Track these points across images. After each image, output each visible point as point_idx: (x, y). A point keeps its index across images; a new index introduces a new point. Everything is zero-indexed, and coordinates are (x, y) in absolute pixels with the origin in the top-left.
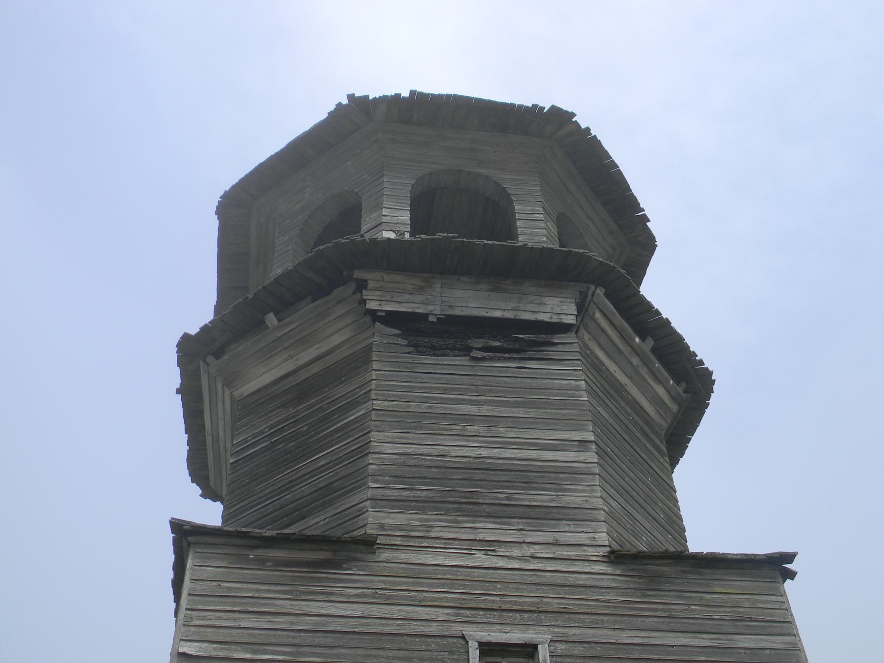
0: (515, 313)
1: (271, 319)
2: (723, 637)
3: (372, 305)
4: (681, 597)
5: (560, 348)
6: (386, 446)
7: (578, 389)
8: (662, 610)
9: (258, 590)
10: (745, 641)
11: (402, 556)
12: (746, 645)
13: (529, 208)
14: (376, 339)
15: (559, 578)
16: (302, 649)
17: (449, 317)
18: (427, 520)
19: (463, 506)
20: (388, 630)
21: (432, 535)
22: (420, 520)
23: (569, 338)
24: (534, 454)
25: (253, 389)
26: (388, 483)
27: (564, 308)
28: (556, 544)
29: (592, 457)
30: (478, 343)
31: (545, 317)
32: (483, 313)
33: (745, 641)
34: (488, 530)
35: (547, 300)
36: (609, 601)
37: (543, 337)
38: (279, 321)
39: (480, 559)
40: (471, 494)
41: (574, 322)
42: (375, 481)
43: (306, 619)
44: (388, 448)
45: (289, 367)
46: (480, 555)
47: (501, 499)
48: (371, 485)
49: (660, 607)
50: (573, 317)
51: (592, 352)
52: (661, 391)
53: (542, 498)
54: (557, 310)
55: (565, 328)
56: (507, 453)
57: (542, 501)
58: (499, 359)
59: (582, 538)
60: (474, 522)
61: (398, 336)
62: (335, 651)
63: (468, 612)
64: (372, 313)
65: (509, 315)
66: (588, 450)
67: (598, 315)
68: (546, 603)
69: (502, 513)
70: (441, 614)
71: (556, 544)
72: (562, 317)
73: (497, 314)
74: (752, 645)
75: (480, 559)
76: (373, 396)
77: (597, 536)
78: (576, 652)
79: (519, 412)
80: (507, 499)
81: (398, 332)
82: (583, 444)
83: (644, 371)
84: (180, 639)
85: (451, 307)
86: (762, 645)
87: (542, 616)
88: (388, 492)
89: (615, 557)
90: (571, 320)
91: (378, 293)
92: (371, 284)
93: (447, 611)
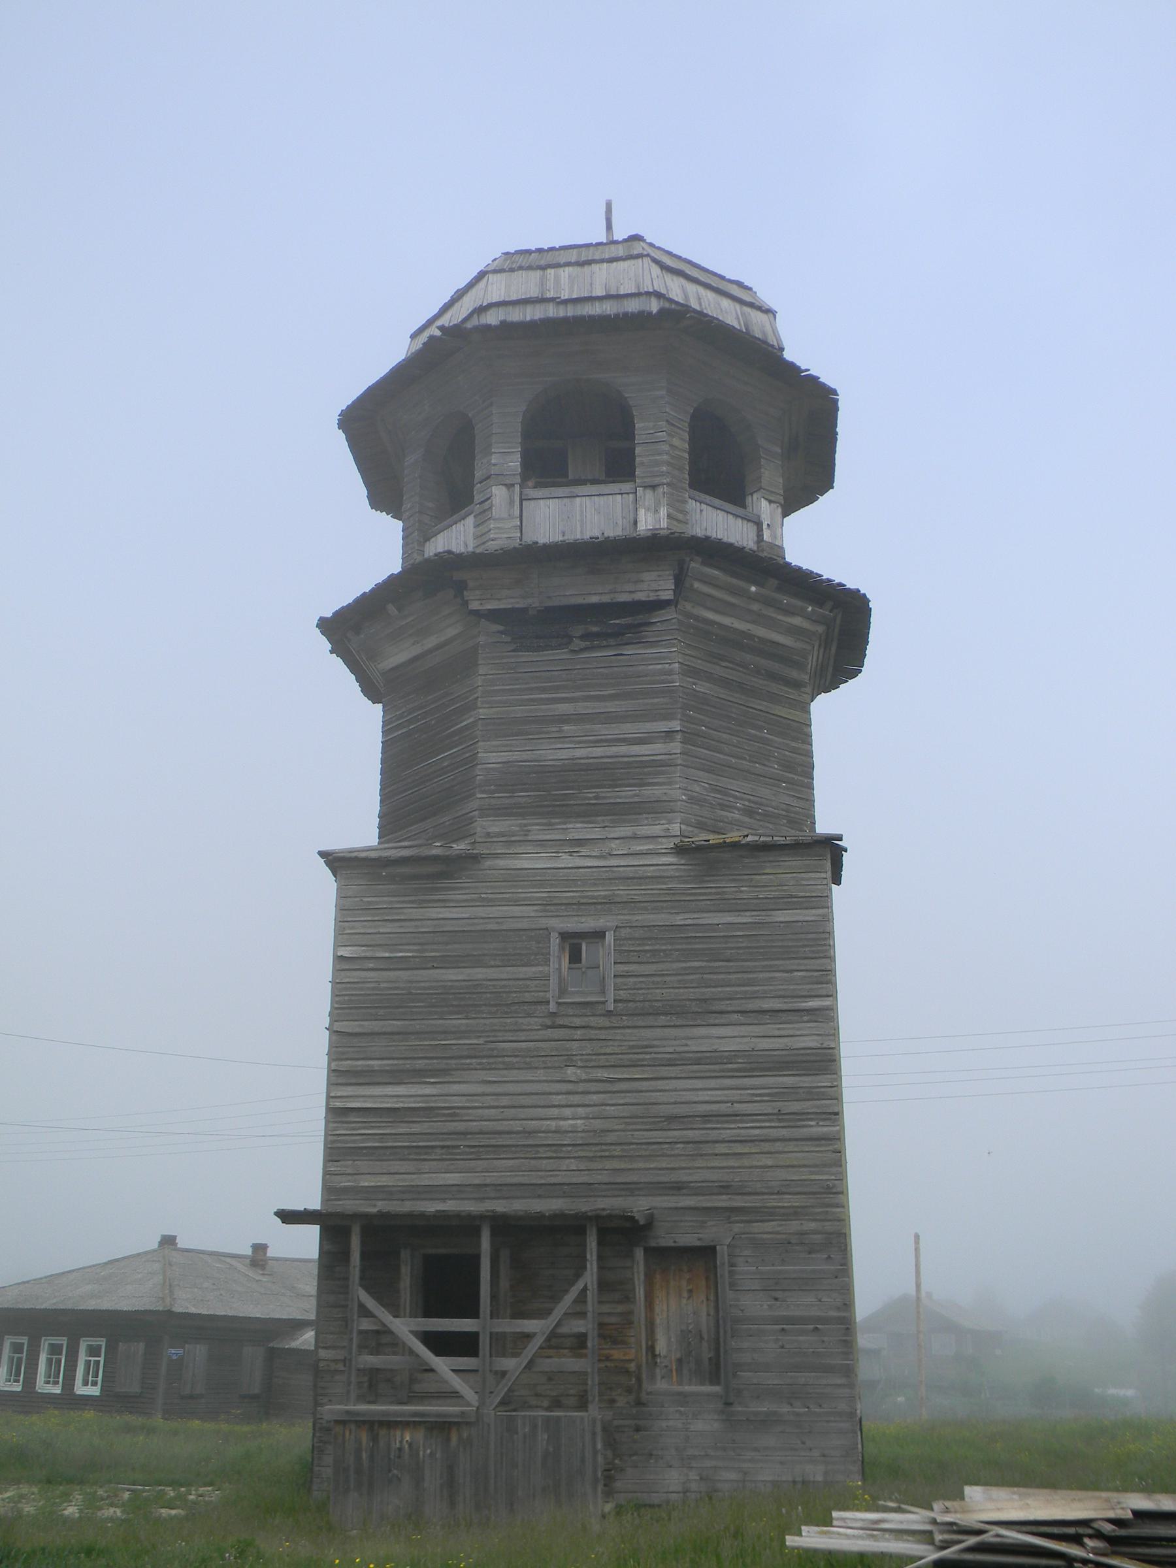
0: (612, 596)
1: (391, 609)
2: (764, 913)
3: (474, 605)
4: (734, 880)
5: (660, 627)
6: (493, 756)
7: (670, 672)
8: (715, 894)
9: (392, 902)
10: (781, 916)
11: (501, 863)
12: (782, 919)
13: (651, 424)
14: (482, 639)
15: (630, 872)
16: (426, 947)
17: (548, 609)
18: (525, 825)
19: (557, 809)
20: (489, 927)
21: (530, 838)
22: (520, 825)
23: (669, 614)
24: (623, 749)
25: (391, 666)
26: (493, 792)
27: (661, 582)
28: (635, 837)
29: (676, 747)
30: (578, 630)
31: (641, 596)
32: (579, 600)
33: (781, 916)
34: (578, 830)
35: (646, 576)
36: (670, 889)
37: (640, 619)
38: (399, 610)
39: (566, 861)
40: (560, 795)
41: (672, 597)
42: (483, 792)
43: (429, 922)
44: (494, 757)
45: (416, 650)
46: (565, 856)
47: (590, 799)
48: (479, 796)
49: (713, 890)
50: (671, 592)
51: (697, 618)
52: (797, 621)
53: (625, 794)
54: (654, 586)
55: (660, 605)
56: (598, 751)
57: (626, 797)
58: (600, 647)
59: (657, 830)
60: (565, 823)
61: (501, 632)
62: (449, 947)
63: (552, 908)
64: (476, 613)
65: (606, 599)
66: (673, 740)
67: (697, 585)
68: (617, 895)
69: (589, 813)
70: (530, 911)
71: (635, 837)
72: (659, 593)
73: (594, 599)
74: (788, 919)
75: (566, 861)
76: (479, 704)
77: (671, 827)
78: (637, 935)
79: (611, 707)
80: (596, 798)
81: (501, 628)
82: (669, 735)
83: (770, 612)
84: (336, 946)
85: (549, 597)
86: (801, 918)
87: (613, 907)
88: (493, 802)
89: (680, 850)
90: (668, 595)
91: (478, 592)
92: (471, 584)
93: (536, 908)
